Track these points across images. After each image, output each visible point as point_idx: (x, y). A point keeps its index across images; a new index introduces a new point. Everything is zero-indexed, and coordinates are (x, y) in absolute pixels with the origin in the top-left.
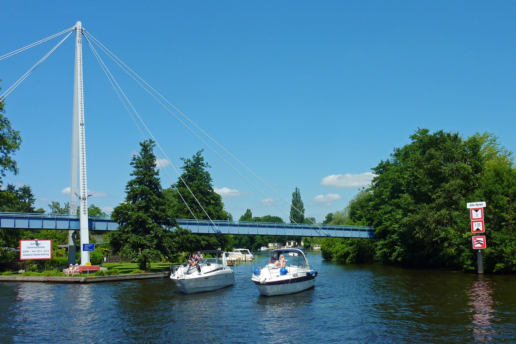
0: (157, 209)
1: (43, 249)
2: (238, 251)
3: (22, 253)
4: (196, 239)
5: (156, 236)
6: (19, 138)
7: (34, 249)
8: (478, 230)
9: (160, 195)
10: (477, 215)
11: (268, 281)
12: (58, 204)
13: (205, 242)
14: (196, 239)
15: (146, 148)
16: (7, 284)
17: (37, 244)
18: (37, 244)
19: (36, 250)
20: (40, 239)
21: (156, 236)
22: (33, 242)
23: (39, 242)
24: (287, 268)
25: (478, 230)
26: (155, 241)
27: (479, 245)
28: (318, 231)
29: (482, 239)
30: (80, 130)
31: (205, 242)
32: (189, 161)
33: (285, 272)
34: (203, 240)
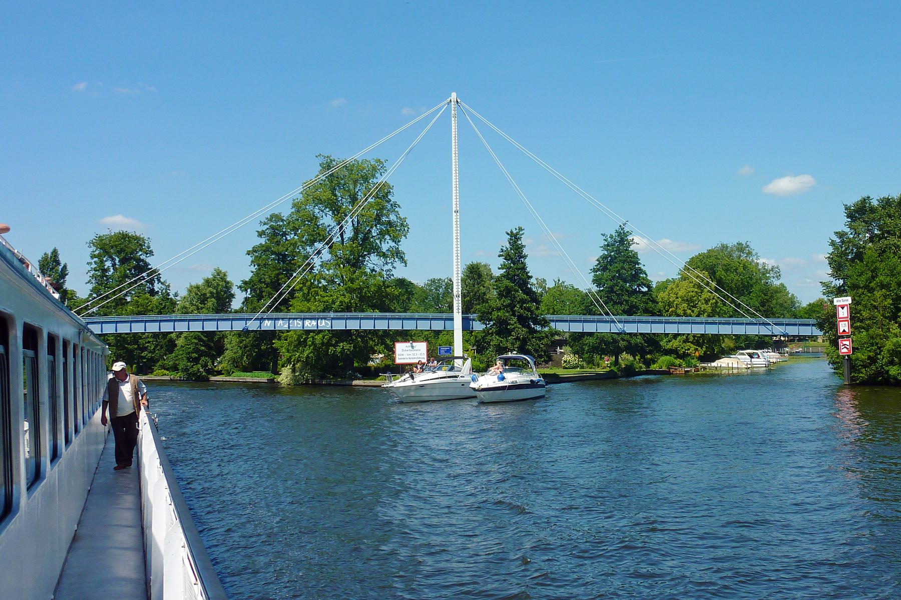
0: (521, 307)
1: (418, 352)
2: (743, 354)
3: (397, 357)
4: (613, 339)
5: (517, 339)
6: (407, 225)
7: (409, 352)
8: (844, 331)
9: (529, 292)
10: (843, 313)
11: (482, 387)
12: (545, 281)
13: (625, 343)
14: (613, 339)
15: (515, 238)
16: (369, 388)
17: (412, 347)
18: (412, 347)
19: (411, 353)
20: (414, 341)
21: (517, 339)
22: (409, 344)
23: (414, 344)
24: (505, 375)
25: (844, 331)
26: (518, 344)
27: (845, 350)
28: (770, 327)
29: (847, 343)
30: (454, 217)
31: (625, 343)
32: (611, 237)
33: (503, 379)
34: (623, 340)
